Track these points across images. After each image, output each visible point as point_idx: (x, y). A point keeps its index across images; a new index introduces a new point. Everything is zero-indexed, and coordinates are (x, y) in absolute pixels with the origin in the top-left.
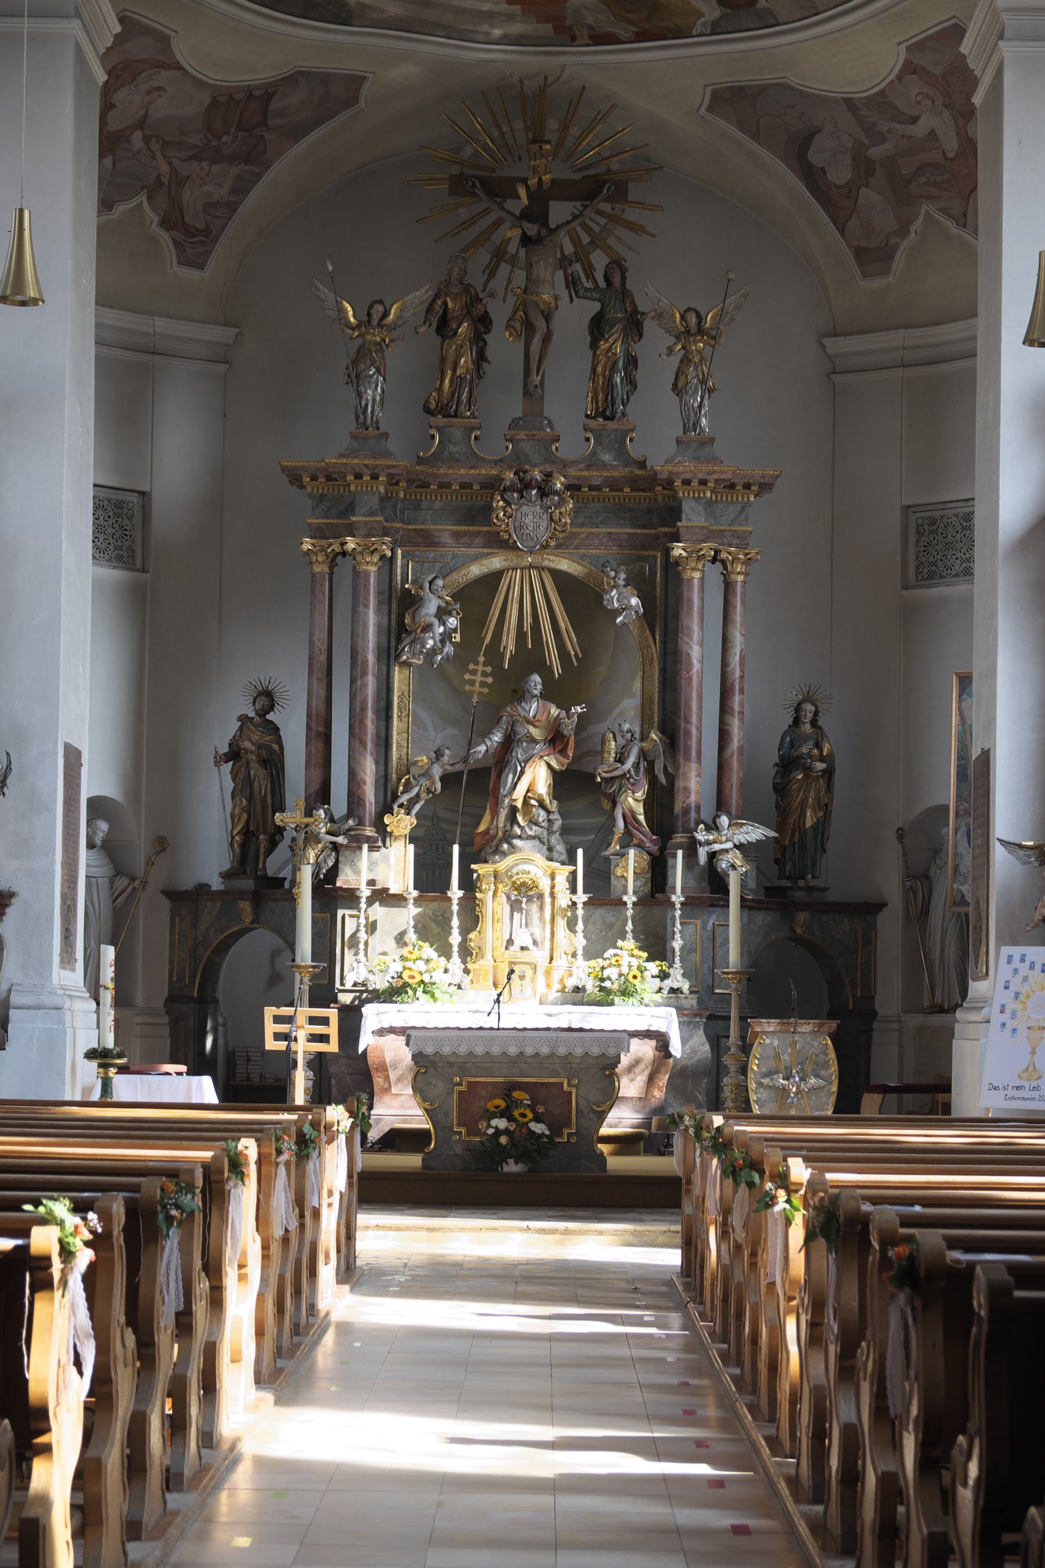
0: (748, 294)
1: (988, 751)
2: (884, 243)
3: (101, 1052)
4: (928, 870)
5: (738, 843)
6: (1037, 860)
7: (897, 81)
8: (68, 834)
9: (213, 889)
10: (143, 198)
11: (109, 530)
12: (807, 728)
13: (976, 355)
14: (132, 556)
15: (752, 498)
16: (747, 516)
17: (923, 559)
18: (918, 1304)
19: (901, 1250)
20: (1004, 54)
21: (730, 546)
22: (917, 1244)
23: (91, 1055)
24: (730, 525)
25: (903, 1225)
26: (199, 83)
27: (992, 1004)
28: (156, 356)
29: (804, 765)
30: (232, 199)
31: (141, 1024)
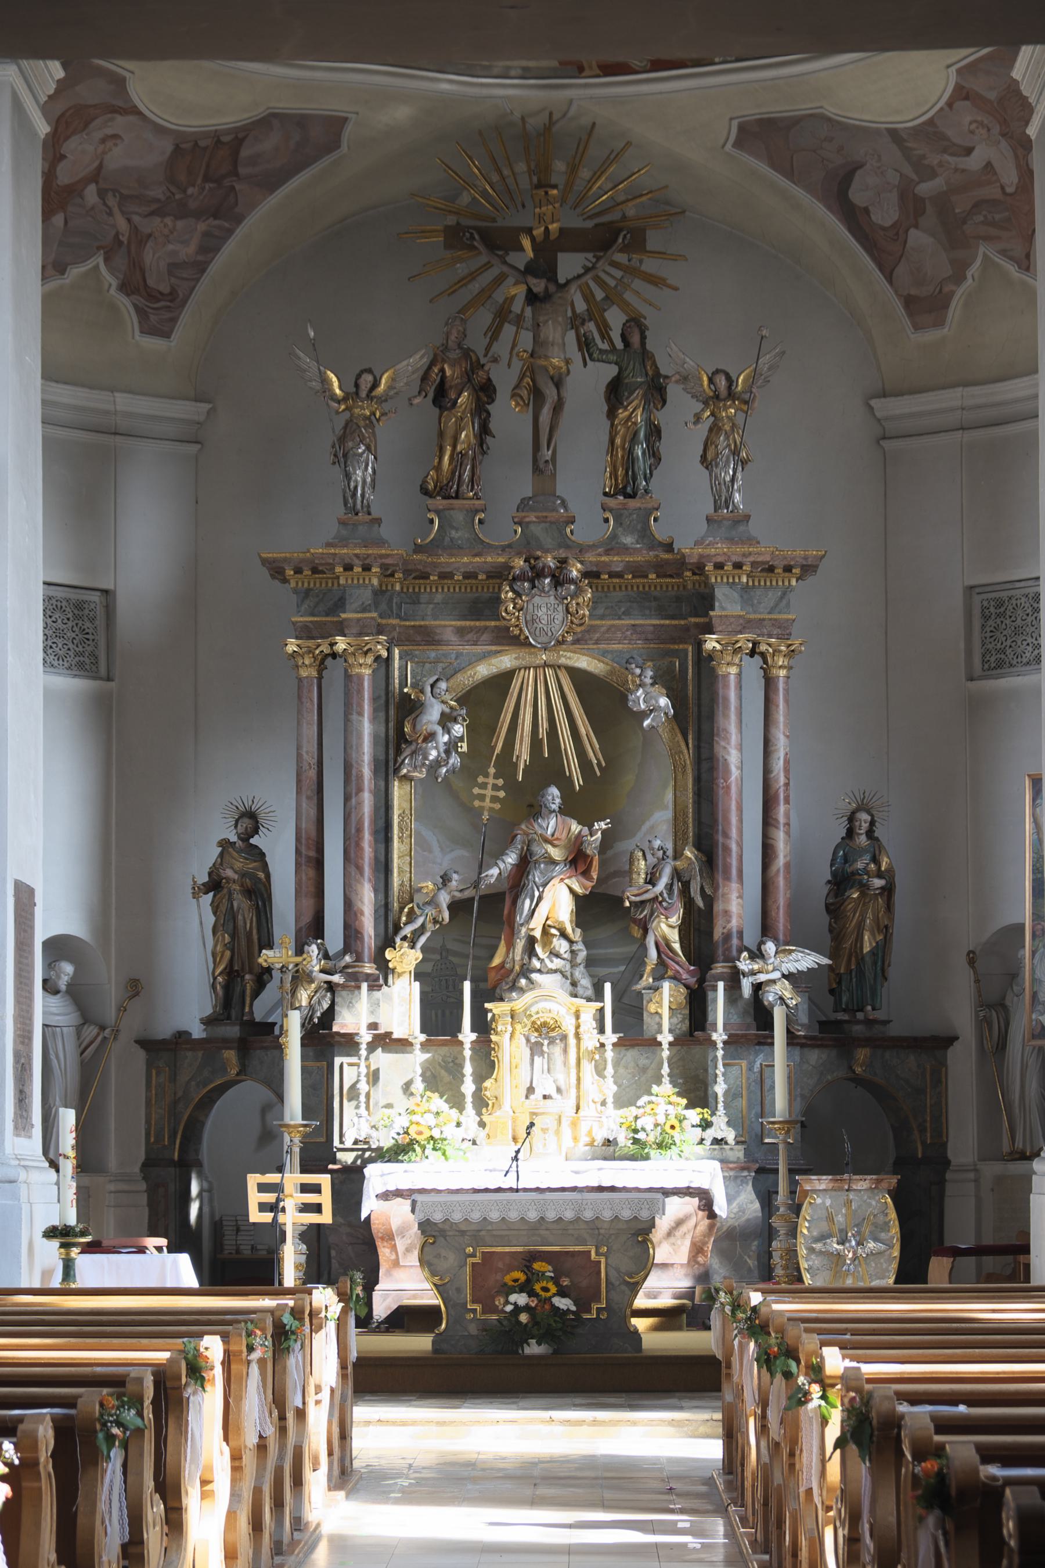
0: (783, 353)
3: (62, 1229)
4: (1004, 998)
5: (786, 973)
7: (947, 109)
8: (21, 983)
9: (193, 1037)
10: (99, 260)
11: (69, 634)
12: (862, 840)
14: (96, 663)
15: (794, 582)
17: (990, 646)
18: (950, 1526)
19: (929, 1466)
21: (770, 636)
22: (947, 1458)
23: (51, 1233)
24: (769, 613)
26: (160, 130)
28: (118, 437)
30: (200, 258)
31: (115, 1192)
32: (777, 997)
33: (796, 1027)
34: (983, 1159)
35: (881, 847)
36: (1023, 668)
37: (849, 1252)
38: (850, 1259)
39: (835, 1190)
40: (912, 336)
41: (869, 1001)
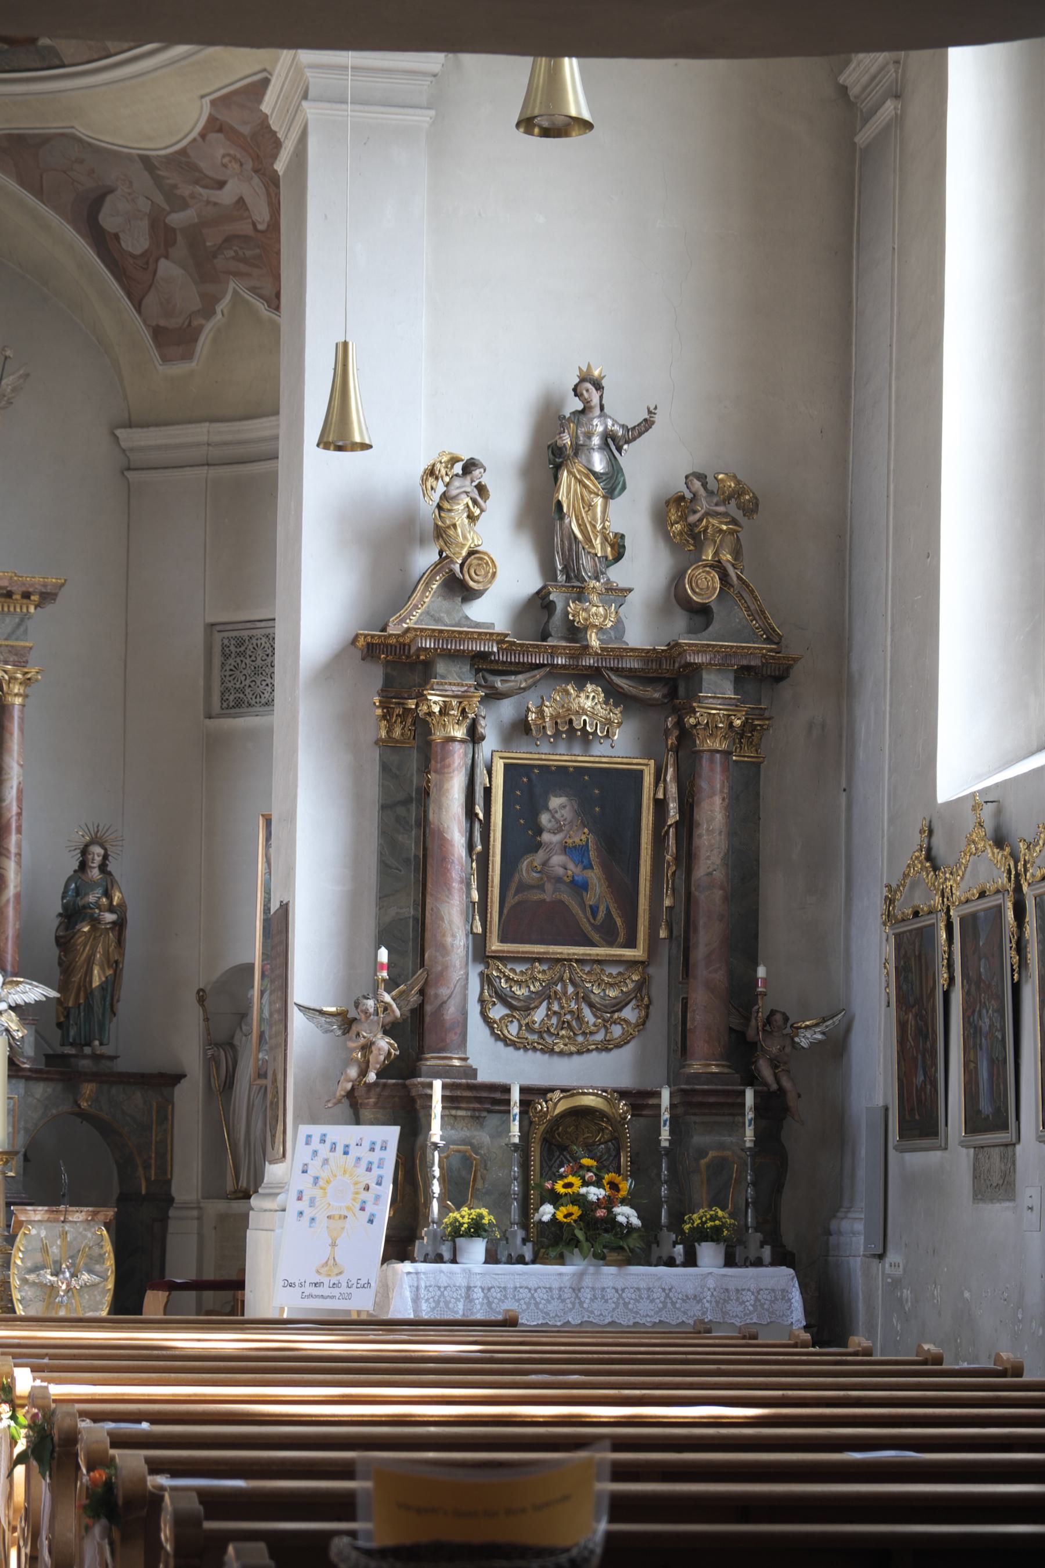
0: (28, 375)
1: (287, 904)
2: (186, 323)
4: (232, 1037)
5: (13, 1004)
6: (340, 1028)
7: (199, 139)
12: (95, 873)
13: (277, 458)
15: (32, 609)
16: (26, 630)
17: (229, 685)
18: (116, 1535)
19: (97, 1475)
20: (309, 116)
21: (6, 663)
22: (116, 1468)
24: (6, 639)
25: (114, 1445)
27: (288, 1190)
29: (92, 916)
32: (3, 1028)
33: (22, 1059)
34: (207, 1196)
35: (113, 882)
36: (261, 709)
37: (62, 1283)
38: (63, 1291)
39: (51, 1221)
40: (160, 368)
41: (97, 1036)
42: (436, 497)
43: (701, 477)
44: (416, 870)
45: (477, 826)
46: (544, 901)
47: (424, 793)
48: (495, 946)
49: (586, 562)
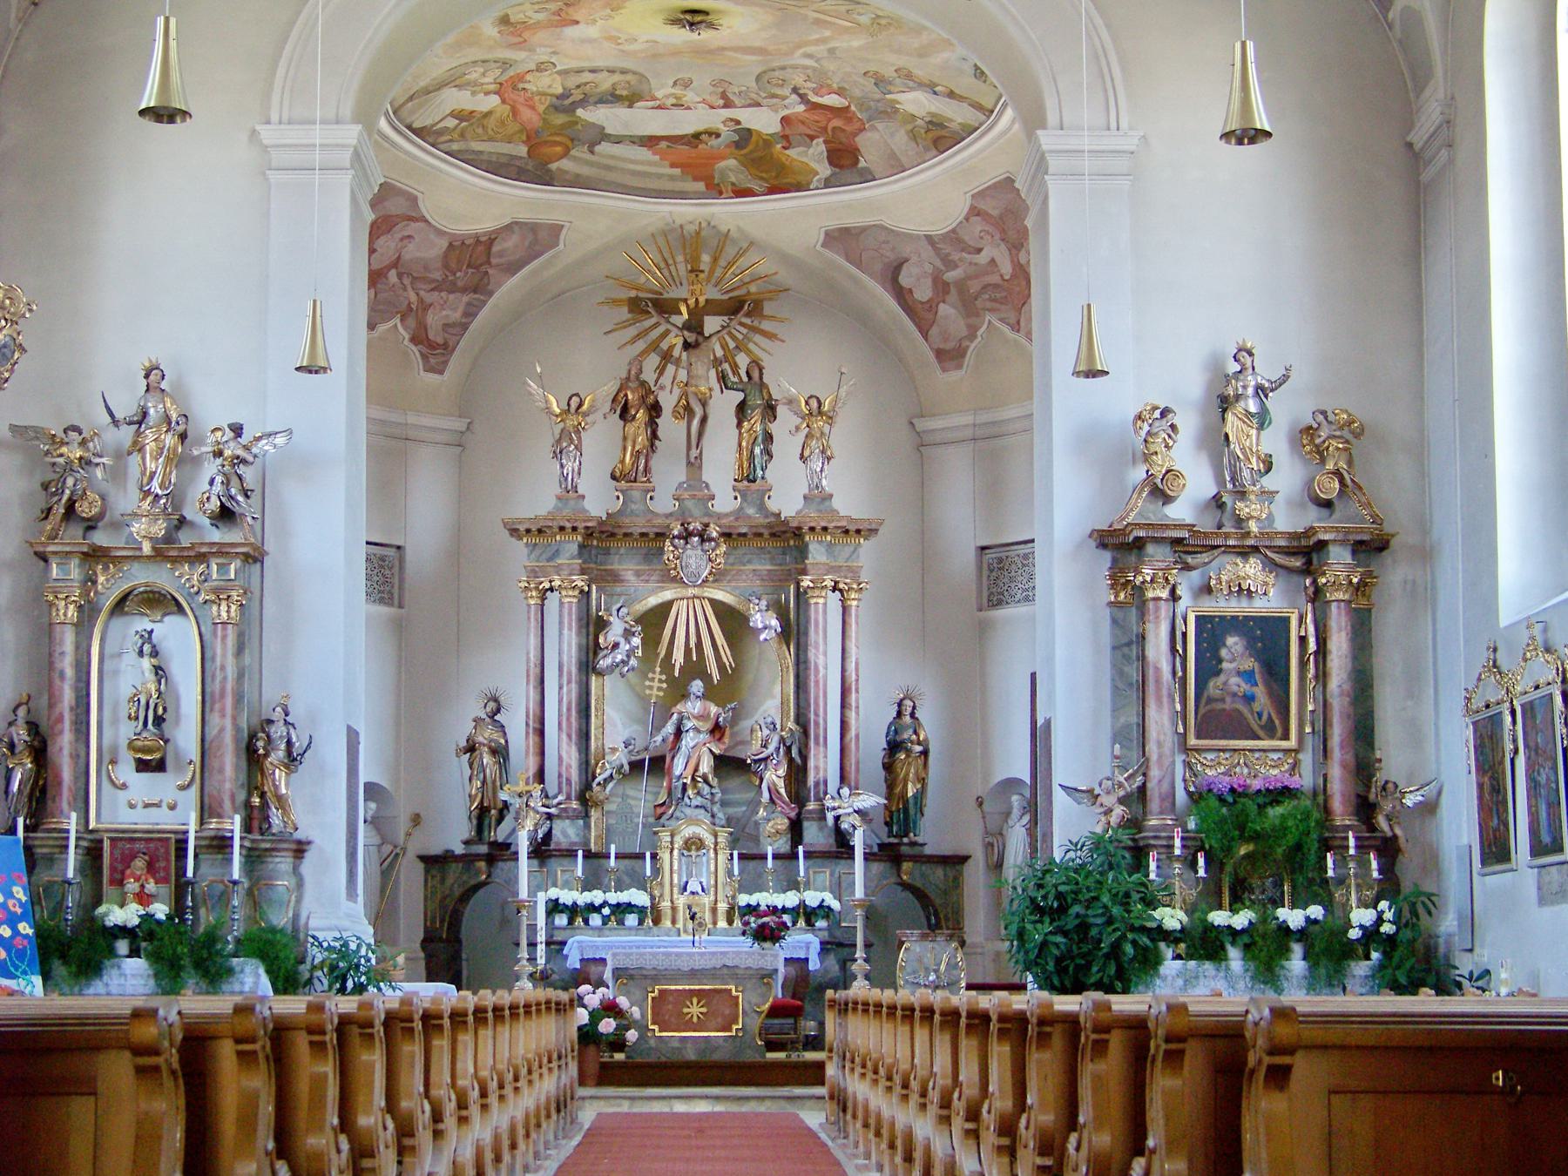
10: (397, 320)
12: (907, 719)
14: (391, 598)
26: (440, 233)
35: (920, 724)
42: (1143, 433)
43: (1324, 413)
44: (1138, 689)
45: (1178, 659)
46: (1224, 710)
47: (1142, 638)
48: (1192, 741)
49: (1246, 473)
